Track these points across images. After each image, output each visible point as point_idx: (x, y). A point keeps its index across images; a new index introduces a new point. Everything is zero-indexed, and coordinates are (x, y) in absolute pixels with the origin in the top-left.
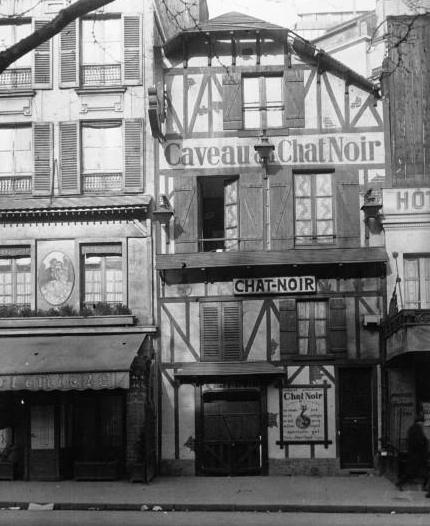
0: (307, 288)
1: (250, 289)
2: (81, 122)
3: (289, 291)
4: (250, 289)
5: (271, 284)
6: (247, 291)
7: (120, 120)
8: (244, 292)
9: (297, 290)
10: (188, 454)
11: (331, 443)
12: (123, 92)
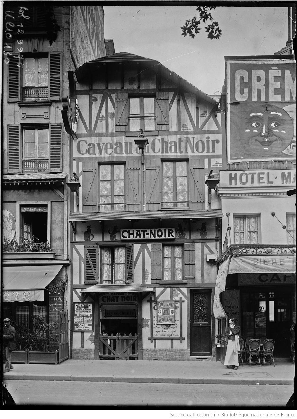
0: (169, 236)
1: (131, 236)
2: (22, 125)
3: (157, 238)
4: (131, 236)
5: (146, 233)
6: (129, 237)
7: (47, 124)
8: (128, 238)
9: (163, 237)
10: (90, 346)
11: (184, 339)
12: (50, 106)
